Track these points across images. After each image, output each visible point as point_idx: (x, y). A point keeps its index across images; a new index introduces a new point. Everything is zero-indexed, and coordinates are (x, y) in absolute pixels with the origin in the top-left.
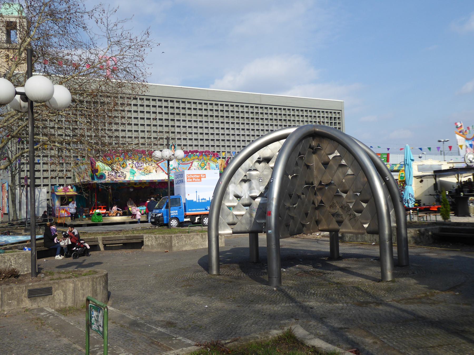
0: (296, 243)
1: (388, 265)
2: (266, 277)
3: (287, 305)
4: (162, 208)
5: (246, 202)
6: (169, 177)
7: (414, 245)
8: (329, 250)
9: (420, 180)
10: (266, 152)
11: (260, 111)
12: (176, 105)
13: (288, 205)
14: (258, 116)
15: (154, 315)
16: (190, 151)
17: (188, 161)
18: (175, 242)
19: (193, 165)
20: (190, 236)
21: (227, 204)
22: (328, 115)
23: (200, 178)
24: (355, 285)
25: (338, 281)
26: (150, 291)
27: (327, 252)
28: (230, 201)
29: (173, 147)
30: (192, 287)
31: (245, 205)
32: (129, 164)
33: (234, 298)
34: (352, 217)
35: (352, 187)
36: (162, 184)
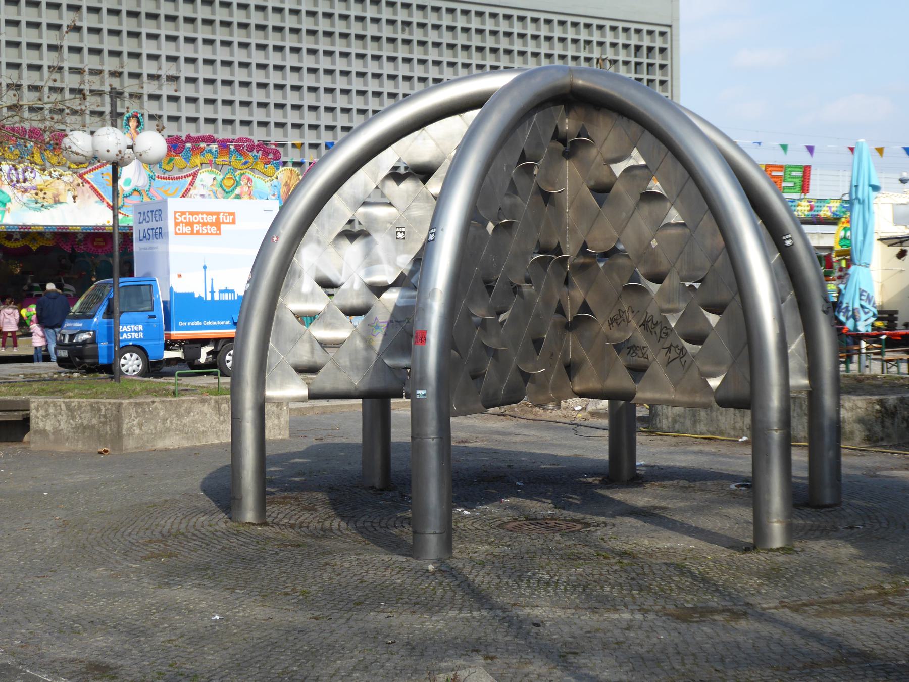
0: (509, 434)
1: (776, 501)
2: (406, 533)
3: (465, 614)
4: (92, 317)
5: (355, 301)
6: (115, 217)
7: (864, 446)
9: (897, 249)
13: (480, 312)
14: (411, 33)
15: (49, 643)
16: (188, 137)
17: (181, 170)
18: (131, 422)
19: (198, 182)
20: (179, 404)
21: (292, 304)
22: (629, 38)
23: (217, 223)
24: (674, 560)
25: (627, 547)
26: (42, 570)
27: (602, 461)
28: (303, 297)
29: (133, 123)
30: (172, 558)
31: (351, 312)
33: (304, 593)
34: (673, 354)
35: (678, 265)
36: (97, 238)
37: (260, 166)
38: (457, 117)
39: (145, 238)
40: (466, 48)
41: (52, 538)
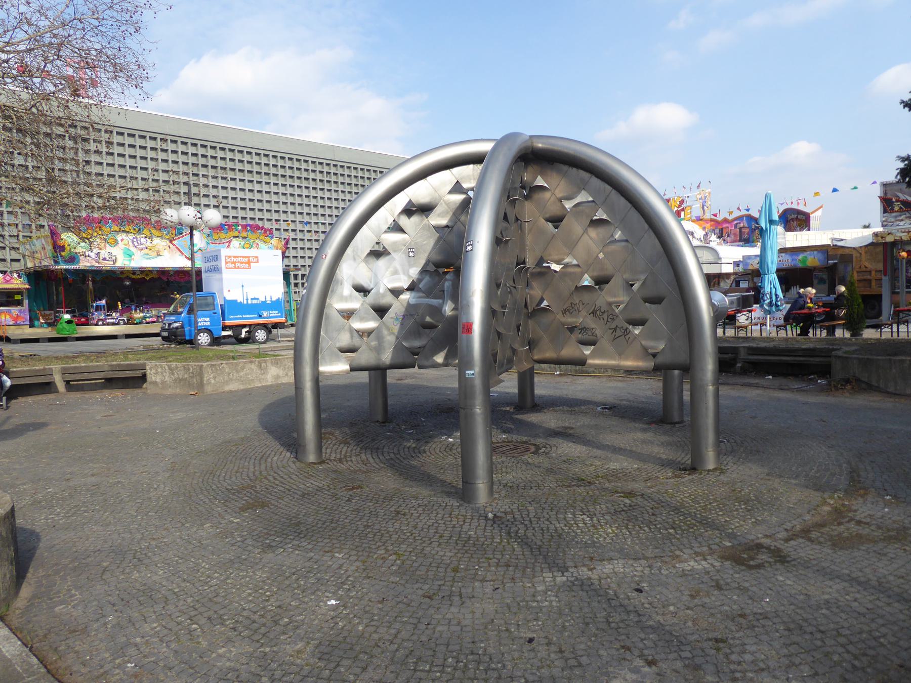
8: (516, 391)
10: (419, 192)
11: (333, 170)
12: (201, 151)
18: (209, 376)
20: (237, 365)
21: (337, 304)
23: (249, 262)
32: (122, 240)
36: (181, 273)
37: (263, 238)
38: (448, 171)
39: (209, 271)
40: (356, 185)
41: (164, 483)
